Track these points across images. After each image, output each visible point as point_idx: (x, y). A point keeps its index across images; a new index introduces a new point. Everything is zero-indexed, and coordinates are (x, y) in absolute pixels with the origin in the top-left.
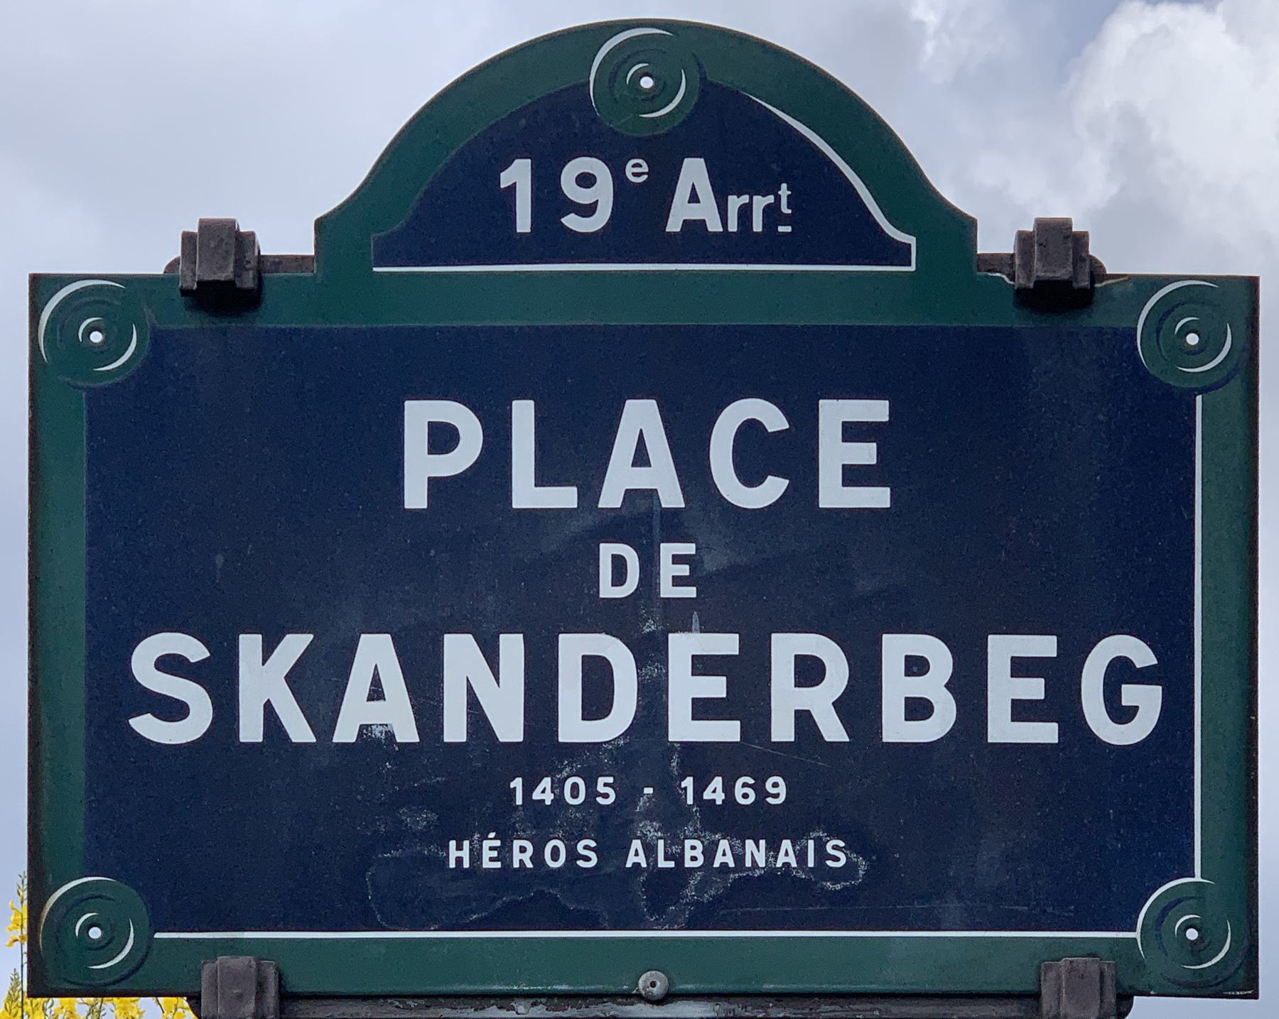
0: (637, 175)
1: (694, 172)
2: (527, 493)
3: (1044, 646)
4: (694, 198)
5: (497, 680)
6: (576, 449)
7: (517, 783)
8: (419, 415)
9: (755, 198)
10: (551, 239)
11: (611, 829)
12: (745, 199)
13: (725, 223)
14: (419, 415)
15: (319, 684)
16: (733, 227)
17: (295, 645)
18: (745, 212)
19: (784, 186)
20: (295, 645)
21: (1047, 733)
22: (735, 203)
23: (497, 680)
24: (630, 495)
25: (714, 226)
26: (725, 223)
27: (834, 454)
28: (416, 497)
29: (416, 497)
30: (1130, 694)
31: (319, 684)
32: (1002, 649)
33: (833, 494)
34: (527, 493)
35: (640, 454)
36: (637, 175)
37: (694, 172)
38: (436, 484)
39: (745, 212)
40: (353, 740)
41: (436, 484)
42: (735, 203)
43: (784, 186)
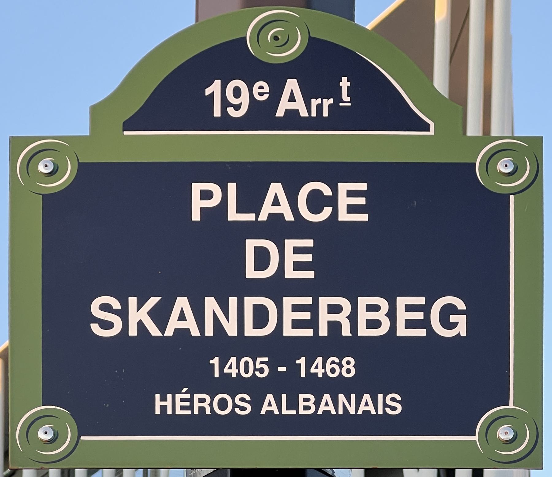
0: (261, 94)
1: (292, 85)
2: (233, 215)
3: (421, 301)
4: (292, 97)
5: (213, 311)
6: (250, 201)
7: (215, 361)
8: (197, 188)
9: (324, 100)
10: (227, 122)
11: (256, 389)
12: (319, 101)
13: (309, 111)
14: (197, 188)
15: (160, 316)
16: (314, 114)
17: (153, 301)
18: (320, 108)
19: (345, 79)
20: (153, 301)
21: (422, 332)
22: (315, 102)
23: (213, 311)
24: (270, 215)
25: (304, 113)
26: (309, 111)
27: (344, 201)
28: (196, 216)
29: (196, 216)
30: (453, 318)
31: (160, 316)
32: (402, 302)
33: (344, 216)
34: (233, 215)
35: (275, 201)
36: (261, 94)
37: (292, 85)
38: (203, 210)
39: (320, 108)
40: (172, 335)
41: (203, 210)
42: (315, 102)
43: (345, 79)
